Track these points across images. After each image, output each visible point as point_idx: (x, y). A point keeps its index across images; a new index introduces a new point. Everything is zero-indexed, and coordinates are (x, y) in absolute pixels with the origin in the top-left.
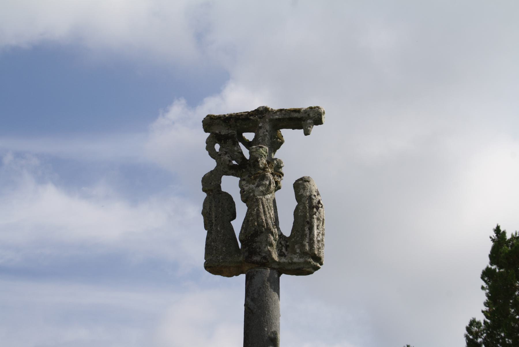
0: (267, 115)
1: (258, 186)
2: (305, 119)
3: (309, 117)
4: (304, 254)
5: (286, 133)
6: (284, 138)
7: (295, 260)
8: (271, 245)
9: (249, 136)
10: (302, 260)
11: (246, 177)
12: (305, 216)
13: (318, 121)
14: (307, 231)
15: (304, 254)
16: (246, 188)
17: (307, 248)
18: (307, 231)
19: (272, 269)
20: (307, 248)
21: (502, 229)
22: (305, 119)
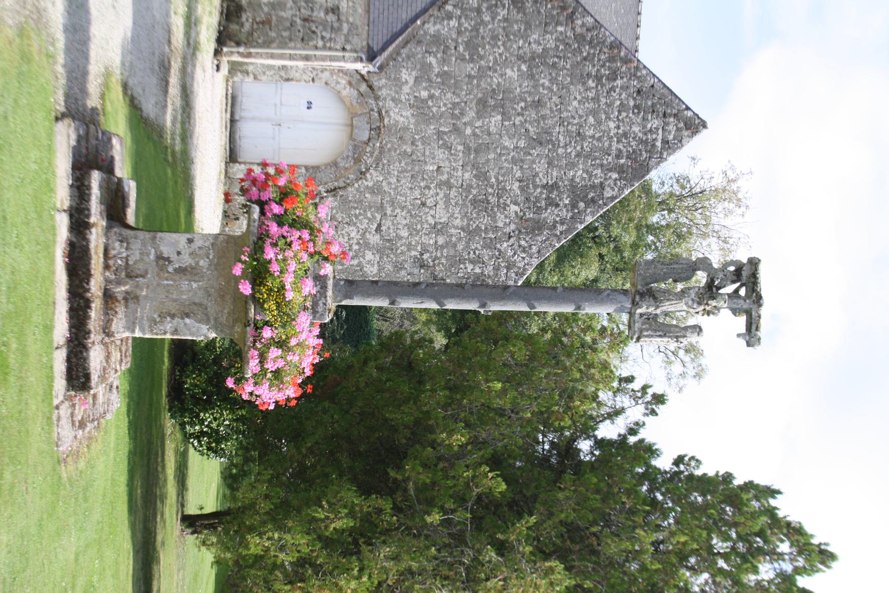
0: (756, 306)
1: (693, 300)
2: (751, 333)
3: (751, 337)
4: (641, 331)
5: (743, 319)
6: (738, 318)
7: (637, 325)
8: (647, 308)
9: (743, 292)
10: (636, 329)
11: (701, 291)
12: (670, 332)
13: (749, 344)
14: (658, 333)
15: (641, 331)
16: (691, 291)
17: (645, 333)
18: (658, 333)
19: (631, 309)
20: (645, 333)
21: (778, 496)
22: (751, 333)
